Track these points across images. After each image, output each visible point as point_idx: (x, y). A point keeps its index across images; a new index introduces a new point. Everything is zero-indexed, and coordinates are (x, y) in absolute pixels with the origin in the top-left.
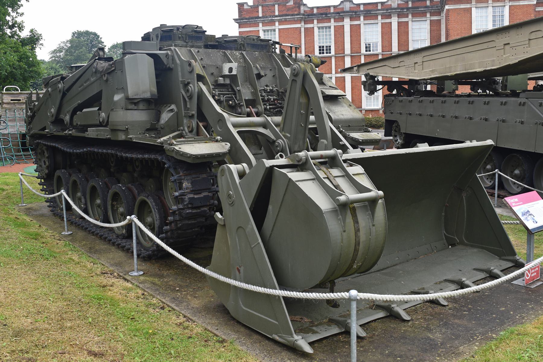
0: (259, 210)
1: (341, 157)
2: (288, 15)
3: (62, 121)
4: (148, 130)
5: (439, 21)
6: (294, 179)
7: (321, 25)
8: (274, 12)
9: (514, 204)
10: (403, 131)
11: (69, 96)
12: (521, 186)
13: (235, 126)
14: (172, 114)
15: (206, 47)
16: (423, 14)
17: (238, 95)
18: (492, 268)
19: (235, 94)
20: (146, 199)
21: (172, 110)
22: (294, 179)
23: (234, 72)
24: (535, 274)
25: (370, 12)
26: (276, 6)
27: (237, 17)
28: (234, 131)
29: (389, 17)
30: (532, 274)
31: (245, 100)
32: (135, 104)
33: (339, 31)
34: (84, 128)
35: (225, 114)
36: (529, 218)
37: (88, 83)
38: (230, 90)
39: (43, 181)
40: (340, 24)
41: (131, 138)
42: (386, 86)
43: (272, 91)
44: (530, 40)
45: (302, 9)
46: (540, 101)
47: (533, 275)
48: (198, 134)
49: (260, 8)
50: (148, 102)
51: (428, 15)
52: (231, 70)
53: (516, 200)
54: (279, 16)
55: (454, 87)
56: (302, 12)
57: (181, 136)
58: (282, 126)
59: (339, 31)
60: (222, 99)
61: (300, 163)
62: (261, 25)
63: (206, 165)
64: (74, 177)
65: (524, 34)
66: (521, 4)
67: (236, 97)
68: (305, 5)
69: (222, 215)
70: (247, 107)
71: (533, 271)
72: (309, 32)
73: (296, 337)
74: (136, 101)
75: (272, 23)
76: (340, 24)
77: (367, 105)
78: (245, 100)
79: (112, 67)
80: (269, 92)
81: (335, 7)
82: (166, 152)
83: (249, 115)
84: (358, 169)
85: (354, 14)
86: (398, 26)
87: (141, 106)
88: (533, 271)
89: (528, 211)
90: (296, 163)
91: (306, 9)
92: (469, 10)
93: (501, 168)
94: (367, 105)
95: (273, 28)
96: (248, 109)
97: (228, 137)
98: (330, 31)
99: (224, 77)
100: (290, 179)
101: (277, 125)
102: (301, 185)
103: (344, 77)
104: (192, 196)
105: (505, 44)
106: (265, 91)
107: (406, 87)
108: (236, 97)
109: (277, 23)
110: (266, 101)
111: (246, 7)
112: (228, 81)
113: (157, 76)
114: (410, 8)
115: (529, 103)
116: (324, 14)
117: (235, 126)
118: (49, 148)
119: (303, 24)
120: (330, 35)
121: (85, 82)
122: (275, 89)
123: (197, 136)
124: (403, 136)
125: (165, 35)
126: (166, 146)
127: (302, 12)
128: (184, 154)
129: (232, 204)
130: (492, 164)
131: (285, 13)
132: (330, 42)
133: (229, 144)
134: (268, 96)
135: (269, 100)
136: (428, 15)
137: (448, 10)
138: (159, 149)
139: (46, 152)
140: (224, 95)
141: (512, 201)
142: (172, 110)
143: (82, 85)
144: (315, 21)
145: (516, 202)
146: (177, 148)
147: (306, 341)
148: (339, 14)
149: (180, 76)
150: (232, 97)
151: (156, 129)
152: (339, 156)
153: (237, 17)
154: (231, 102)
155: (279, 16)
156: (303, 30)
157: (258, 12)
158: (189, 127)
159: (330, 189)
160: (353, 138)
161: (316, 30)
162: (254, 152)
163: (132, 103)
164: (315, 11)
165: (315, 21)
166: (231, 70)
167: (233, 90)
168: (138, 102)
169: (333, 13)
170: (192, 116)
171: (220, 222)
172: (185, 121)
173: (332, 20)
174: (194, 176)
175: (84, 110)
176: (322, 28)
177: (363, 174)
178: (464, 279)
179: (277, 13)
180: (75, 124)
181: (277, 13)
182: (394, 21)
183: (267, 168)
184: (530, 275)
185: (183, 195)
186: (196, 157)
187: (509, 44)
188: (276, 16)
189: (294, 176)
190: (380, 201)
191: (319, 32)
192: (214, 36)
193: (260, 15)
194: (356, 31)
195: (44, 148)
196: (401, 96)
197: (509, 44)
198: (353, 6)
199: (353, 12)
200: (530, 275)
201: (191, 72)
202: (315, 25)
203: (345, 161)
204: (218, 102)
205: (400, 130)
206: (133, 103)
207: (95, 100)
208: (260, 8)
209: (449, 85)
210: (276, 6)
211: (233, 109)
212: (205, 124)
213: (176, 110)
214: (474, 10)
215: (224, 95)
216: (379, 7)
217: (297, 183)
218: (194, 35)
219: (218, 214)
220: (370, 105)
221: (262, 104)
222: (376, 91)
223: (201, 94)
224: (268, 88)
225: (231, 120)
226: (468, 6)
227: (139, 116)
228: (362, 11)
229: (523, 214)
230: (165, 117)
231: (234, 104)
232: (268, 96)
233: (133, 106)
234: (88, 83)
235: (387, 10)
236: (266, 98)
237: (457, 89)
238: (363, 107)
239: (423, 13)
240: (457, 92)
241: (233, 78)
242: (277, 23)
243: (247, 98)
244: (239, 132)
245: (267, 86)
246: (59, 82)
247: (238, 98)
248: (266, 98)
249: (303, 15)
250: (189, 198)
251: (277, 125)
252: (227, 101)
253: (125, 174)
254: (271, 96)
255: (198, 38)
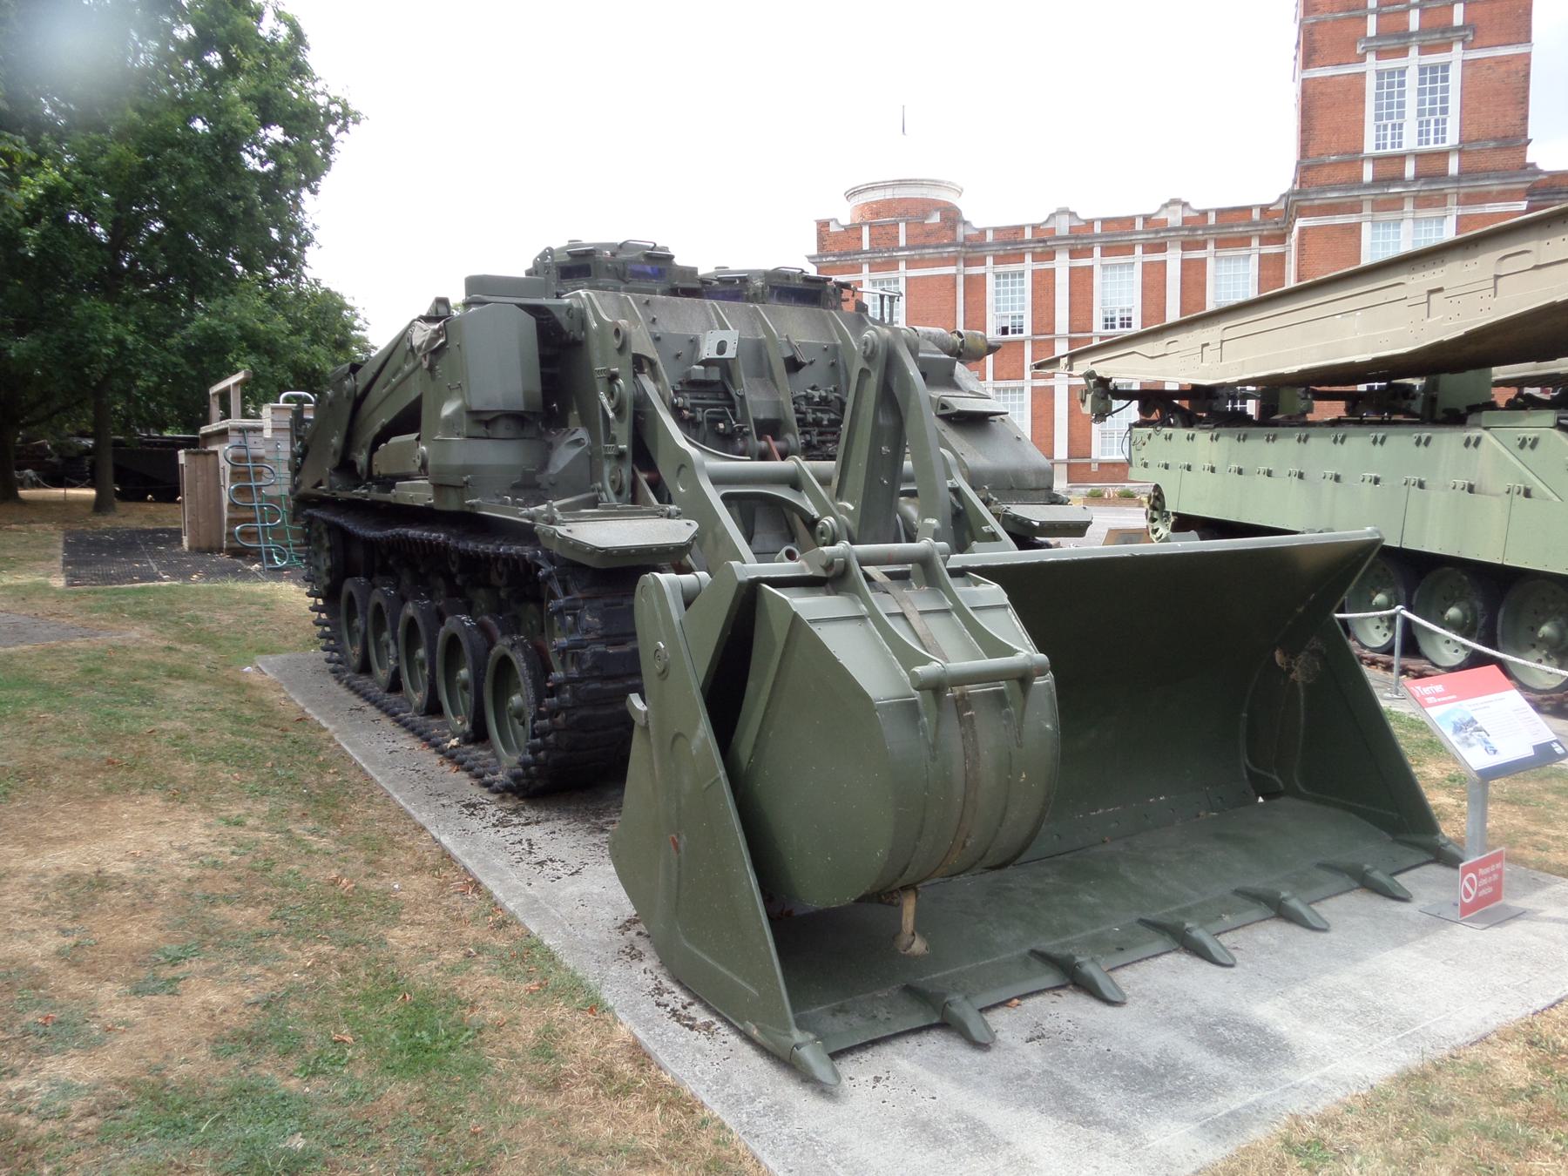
0: (726, 691)
1: (945, 561)
2: (924, 247)
3: (353, 465)
4: (515, 487)
5: (1281, 256)
6: (805, 616)
7: (1002, 268)
8: (897, 238)
9: (1430, 700)
10: (1170, 507)
11: (367, 406)
12: (1464, 647)
13: (717, 480)
14: (578, 450)
15: (674, 292)
16: (1244, 241)
17: (738, 409)
18: (1367, 867)
19: (732, 407)
20: (508, 652)
21: (578, 442)
22: (805, 616)
23: (730, 353)
24: (1490, 890)
25: (1117, 236)
26: (902, 226)
27: (814, 252)
28: (714, 495)
29: (1162, 248)
30: (1479, 889)
31: (756, 421)
32: (487, 424)
33: (1043, 285)
34: (388, 482)
35: (693, 452)
36: (1472, 740)
37: (399, 376)
38: (721, 395)
39: (320, 602)
40: (1047, 265)
41: (472, 506)
42: (1135, 403)
43: (824, 400)
44: (1497, 277)
45: (960, 230)
46: (1522, 435)
47: (1483, 892)
48: (634, 500)
49: (866, 231)
50: (519, 419)
51: (1255, 243)
52: (722, 347)
53: (1439, 688)
54: (907, 248)
55: (1303, 405)
56: (960, 239)
57: (594, 503)
58: (835, 483)
59: (1043, 285)
60: (699, 417)
61: (831, 573)
62: (866, 268)
63: (622, 573)
64: (377, 597)
65: (1484, 263)
66: (1488, 210)
67: (734, 414)
68: (965, 223)
69: (644, 700)
70: (760, 438)
71: (1484, 881)
72: (975, 286)
73: (797, 1036)
74: (487, 417)
75: (891, 264)
76: (1047, 265)
77: (1103, 453)
78: (756, 421)
79: (439, 337)
80: (818, 404)
81: (1035, 227)
82: (542, 541)
83: (764, 456)
84: (993, 592)
85: (1081, 240)
86: (1182, 269)
87: (501, 429)
88: (1484, 881)
89: (1473, 721)
90: (822, 573)
91: (969, 232)
92: (1355, 229)
93: (1414, 602)
94: (1103, 453)
95: (893, 275)
96: (763, 444)
97: (697, 508)
98: (1022, 283)
99: (707, 363)
100: (795, 615)
101: (825, 481)
102: (825, 634)
103: (1052, 388)
104: (600, 648)
105: (1431, 292)
106: (808, 399)
107: (1186, 404)
108: (734, 414)
109: (902, 265)
110: (811, 425)
111: (833, 228)
112: (715, 374)
113: (545, 361)
114: (1211, 227)
115: (1492, 440)
116: (1011, 244)
117: (717, 480)
118: (333, 528)
119: (961, 266)
120: (1022, 291)
121: (394, 376)
122: (832, 397)
123: (631, 501)
124: (1172, 519)
125: (578, 265)
126: (540, 526)
127: (960, 239)
128: (578, 546)
129: (664, 674)
130: (1390, 591)
131: (921, 240)
132: (1022, 308)
133: (695, 525)
134: (814, 411)
135: (817, 423)
136: (1255, 243)
137: (1303, 231)
138: (526, 534)
139: (325, 536)
140: (705, 407)
141: (1426, 690)
142: (578, 442)
143: (389, 381)
144: (990, 261)
145: (1437, 695)
146: (561, 530)
147: (825, 1046)
148: (1042, 242)
149: (602, 360)
150: (725, 413)
151: (537, 486)
152: (938, 558)
153: (814, 252)
154: (721, 426)
155: (907, 248)
156: (960, 280)
157: (860, 239)
158: (613, 482)
159: (909, 640)
160: (1016, 517)
161: (990, 281)
162: (758, 549)
163: (480, 422)
164: (990, 237)
165: (990, 261)
166: (722, 347)
167: (729, 397)
168: (494, 420)
169: (1030, 242)
170: (621, 456)
171: (639, 721)
172: (607, 469)
173: (1028, 258)
174: (608, 601)
175: (394, 440)
176: (1005, 276)
177: (1005, 607)
178: (1284, 894)
179: (902, 242)
180: (375, 473)
181: (902, 242)
182: (1173, 259)
183: (741, 584)
184: (1473, 893)
185: (581, 645)
186: (607, 553)
187: (1440, 290)
188: (902, 249)
189: (804, 604)
190: (1039, 682)
191: (998, 285)
192: (694, 271)
193: (866, 246)
194: (1081, 282)
195: (323, 527)
196: (1170, 425)
197: (1440, 290)
198: (1076, 224)
199: (1076, 238)
200: (1473, 893)
201: (622, 349)
202: (989, 269)
203: (954, 573)
204: (682, 422)
205: (1163, 506)
206: (483, 422)
207: (409, 420)
208: (866, 231)
209: (1293, 400)
210: (902, 226)
211: (726, 442)
212: (645, 475)
213: (587, 441)
214: (1366, 229)
215: (705, 407)
216: (1139, 225)
217: (815, 628)
218: (650, 270)
219: (636, 701)
220: (1111, 453)
221: (797, 430)
222: (1111, 414)
223: (641, 402)
224: (816, 394)
225: (709, 461)
226: (1352, 219)
227: (499, 455)
228: (1098, 236)
229: (1458, 728)
230: (564, 456)
231: (728, 431)
232: (814, 411)
233: (481, 430)
234: (399, 376)
235: (1157, 232)
236: (810, 417)
237: (1310, 410)
238: (1094, 456)
239: (1242, 239)
240: (1310, 417)
241: (725, 366)
242: (902, 265)
243: (761, 417)
244: (726, 499)
245: (813, 388)
246: (347, 376)
247: (739, 415)
248: (810, 417)
249: (963, 245)
250: (594, 654)
251: (825, 481)
252: (713, 422)
253: (482, 592)
254: (822, 411)
255: (659, 274)
